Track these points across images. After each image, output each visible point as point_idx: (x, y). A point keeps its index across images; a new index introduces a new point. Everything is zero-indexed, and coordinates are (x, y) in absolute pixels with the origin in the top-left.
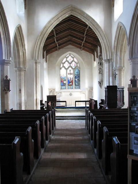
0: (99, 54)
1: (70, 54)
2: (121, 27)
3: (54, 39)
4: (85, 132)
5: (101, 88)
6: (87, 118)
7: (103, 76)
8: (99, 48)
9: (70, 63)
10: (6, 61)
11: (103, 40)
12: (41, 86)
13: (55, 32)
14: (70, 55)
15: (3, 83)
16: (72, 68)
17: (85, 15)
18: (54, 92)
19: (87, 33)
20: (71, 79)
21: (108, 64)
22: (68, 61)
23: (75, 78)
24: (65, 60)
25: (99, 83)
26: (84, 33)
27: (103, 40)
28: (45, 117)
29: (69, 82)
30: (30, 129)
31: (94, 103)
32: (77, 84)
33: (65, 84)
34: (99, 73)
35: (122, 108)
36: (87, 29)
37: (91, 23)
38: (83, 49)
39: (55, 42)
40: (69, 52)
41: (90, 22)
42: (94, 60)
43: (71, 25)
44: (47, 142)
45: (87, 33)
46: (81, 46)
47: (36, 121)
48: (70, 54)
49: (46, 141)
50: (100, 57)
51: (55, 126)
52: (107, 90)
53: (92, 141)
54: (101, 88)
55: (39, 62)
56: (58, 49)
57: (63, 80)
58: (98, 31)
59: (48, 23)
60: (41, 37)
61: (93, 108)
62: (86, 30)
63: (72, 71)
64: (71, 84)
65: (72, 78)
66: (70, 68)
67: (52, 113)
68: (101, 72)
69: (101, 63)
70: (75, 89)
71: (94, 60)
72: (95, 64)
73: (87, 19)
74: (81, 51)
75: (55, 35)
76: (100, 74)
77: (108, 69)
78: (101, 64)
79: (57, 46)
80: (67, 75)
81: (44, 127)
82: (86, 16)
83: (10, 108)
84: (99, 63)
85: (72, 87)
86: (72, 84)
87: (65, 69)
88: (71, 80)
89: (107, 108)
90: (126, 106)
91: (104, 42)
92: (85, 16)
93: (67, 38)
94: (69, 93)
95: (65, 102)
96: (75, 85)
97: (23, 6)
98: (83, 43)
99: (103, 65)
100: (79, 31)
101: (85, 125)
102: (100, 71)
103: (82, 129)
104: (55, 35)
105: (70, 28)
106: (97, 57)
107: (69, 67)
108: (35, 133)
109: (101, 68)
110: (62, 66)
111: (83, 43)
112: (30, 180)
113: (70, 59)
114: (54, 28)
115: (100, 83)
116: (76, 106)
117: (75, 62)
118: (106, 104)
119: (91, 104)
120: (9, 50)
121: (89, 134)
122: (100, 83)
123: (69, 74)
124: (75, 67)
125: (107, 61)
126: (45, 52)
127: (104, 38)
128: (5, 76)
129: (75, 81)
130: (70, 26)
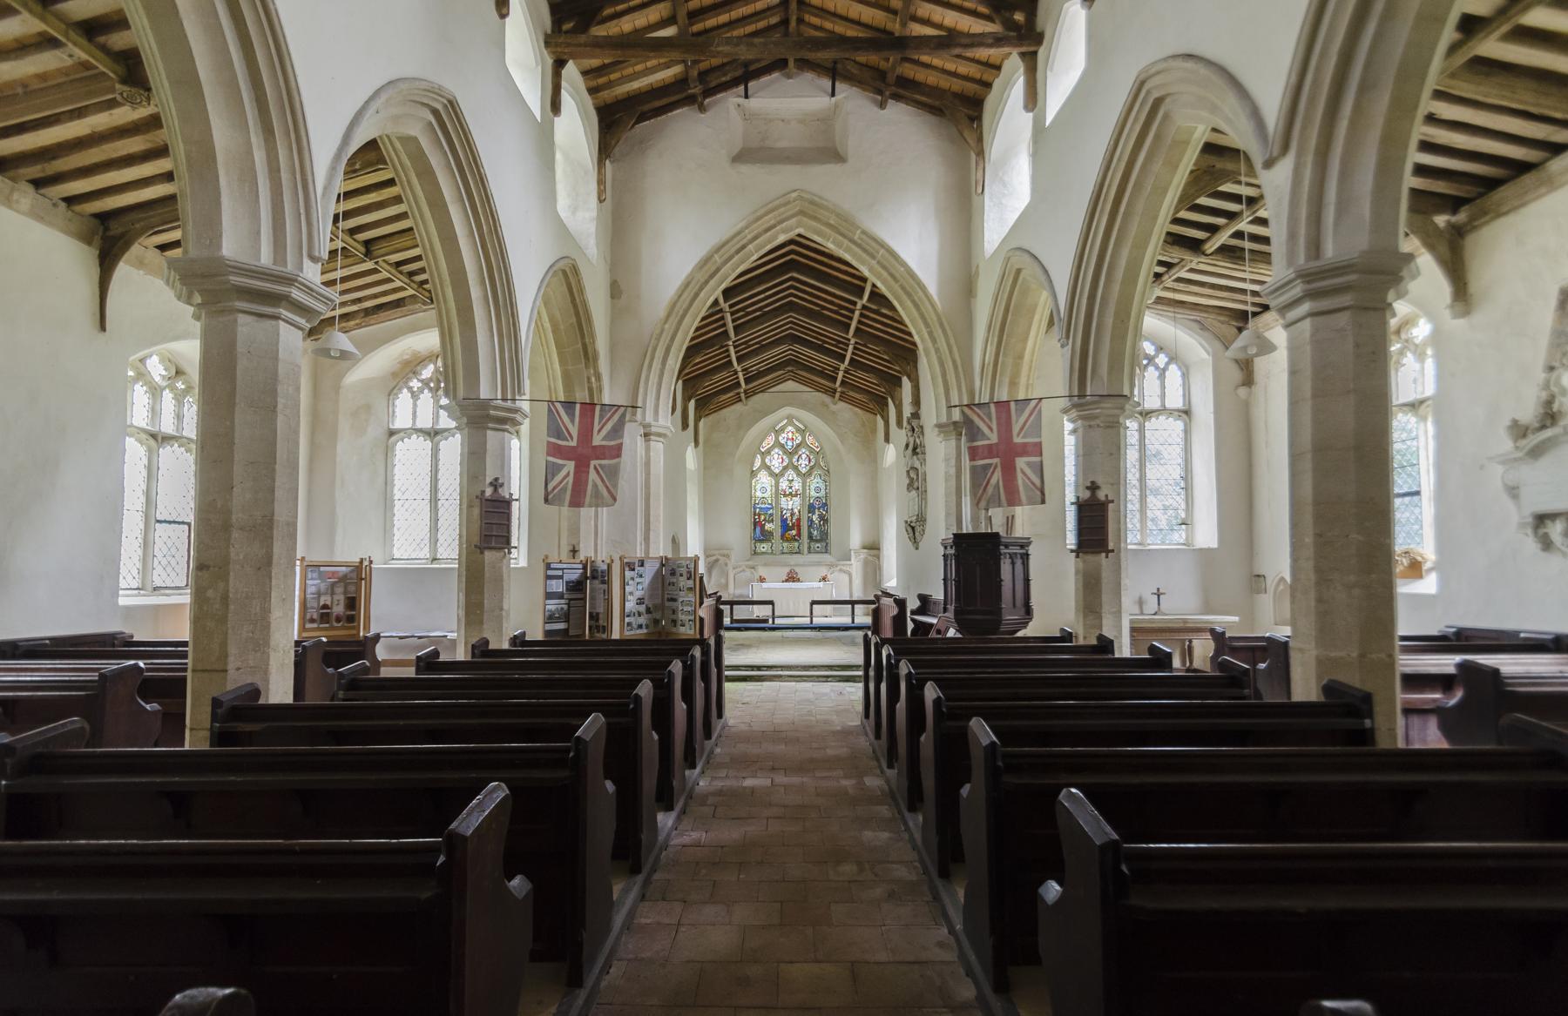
0: (907, 410)
1: (790, 418)
2: (1019, 271)
3: (728, 351)
4: (864, 743)
5: (917, 549)
6: (875, 672)
7: (926, 499)
8: (906, 384)
9: (790, 454)
10: (496, 408)
11: (934, 341)
12: (674, 540)
13: (729, 318)
14: (790, 423)
15: (476, 511)
16: (799, 474)
17: (858, 232)
18: (726, 565)
19: (856, 355)
20: (792, 515)
21: (953, 443)
22: (782, 446)
23: (811, 509)
24: (769, 441)
25: (910, 530)
26: (849, 325)
27: (934, 341)
28: (684, 663)
29: (785, 527)
30: (591, 726)
31: (895, 611)
32: (815, 533)
33: (771, 533)
34: (910, 486)
35: (1020, 634)
36: (864, 307)
37: (884, 267)
38: (844, 398)
39: (730, 362)
40: (787, 410)
41: (878, 262)
42: (887, 440)
43: (795, 323)
44: (665, 820)
45: (856, 355)
46: (835, 383)
47: (635, 683)
48: (790, 418)
49: (660, 817)
50: (914, 424)
51: (720, 716)
52: (953, 551)
53: (916, 821)
54: (917, 549)
55: (659, 435)
56: (743, 395)
57: (762, 518)
58: (914, 302)
59: (701, 268)
60: (667, 326)
61: (888, 632)
62: (859, 306)
63: (797, 485)
64: (794, 532)
65: (796, 511)
66: (791, 474)
67: (705, 653)
68: (915, 482)
69: (915, 449)
70: (809, 552)
71: (887, 440)
72: (891, 455)
73: (865, 251)
74: (835, 404)
75: (732, 333)
76: (914, 492)
77: (953, 462)
78: (916, 450)
79: (738, 384)
80: (777, 497)
81: (680, 707)
82: (859, 238)
83: (511, 629)
84: (907, 446)
85: (796, 544)
86: (799, 534)
87: (772, 474)
88: (795, 518)
89: (951, 633)
90: (1236, 619)
91: (937, 350)
92: (856, 238)
93: (782, 372)
94: (787, 570)
95: (771, 603)
96: (810, 537)
97: (593, 187)
98: (842, 367)
99: (924, 453)
100: (820, 345)
101: (860, 707)
102: (912, 480)
103: (846, 733)
104: (732, 333)
105: (791, 307)
106: (899, 424)
107: (785, 468)
108: (622, 740)
109: (917, 464)
110: (758, 463)
111: (842, 367)
112: (723, 728)
113: (790, 435)
114: (728, 293)
115: (913, 528)
116: (853, 622)
117: (812, 451)
118: (950, 615)
119: (876, 614)
120: (511, 358)
121: (890, 766)
122: (914, 529)
123: (785, 495)
124: (808, 468)
125: (952, 428)
126: (692, 404)
127: (938, 333)
128: (488, 480)
129: (811, 521)
130: (791, 295)
